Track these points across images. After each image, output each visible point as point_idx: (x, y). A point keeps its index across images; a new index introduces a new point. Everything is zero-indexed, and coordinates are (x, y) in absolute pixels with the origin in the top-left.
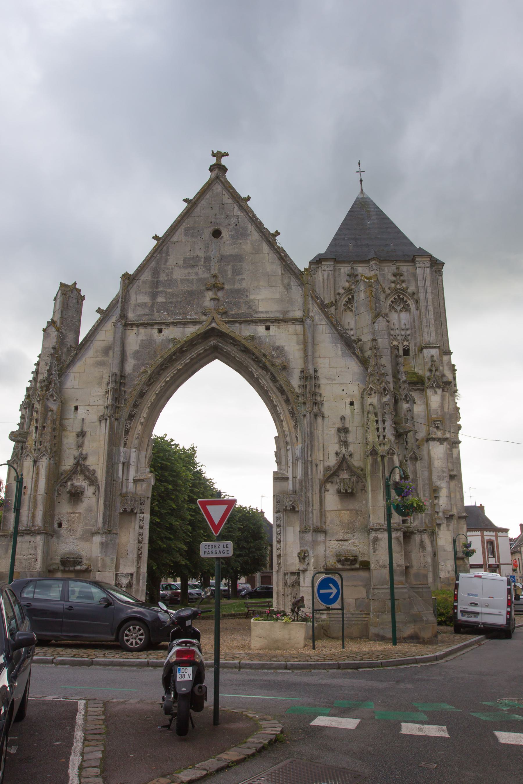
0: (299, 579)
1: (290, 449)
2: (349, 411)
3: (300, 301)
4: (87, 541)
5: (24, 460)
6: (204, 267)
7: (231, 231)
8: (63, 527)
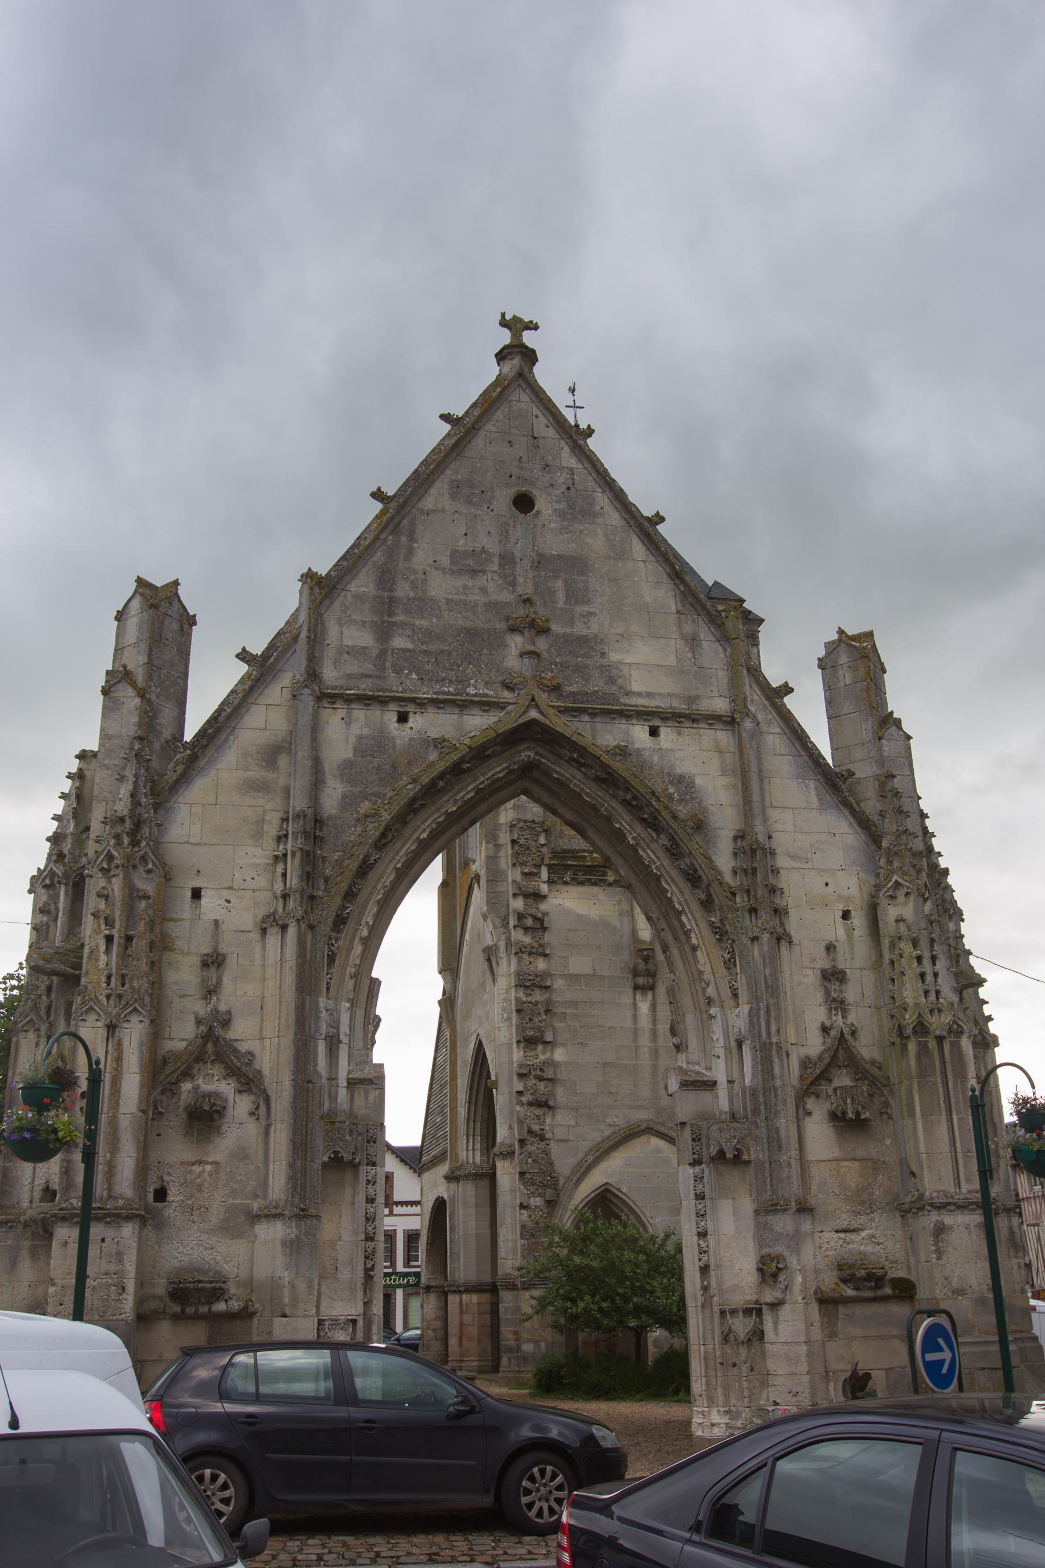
0: (761, 1323)
1: (719, 1015)
2: (841, 934)
3: (723, 676)
4: (237, 1235)
5: (81, 1023)
6: (499, 575)
7: (558, 502)
8: (169, 1198)
